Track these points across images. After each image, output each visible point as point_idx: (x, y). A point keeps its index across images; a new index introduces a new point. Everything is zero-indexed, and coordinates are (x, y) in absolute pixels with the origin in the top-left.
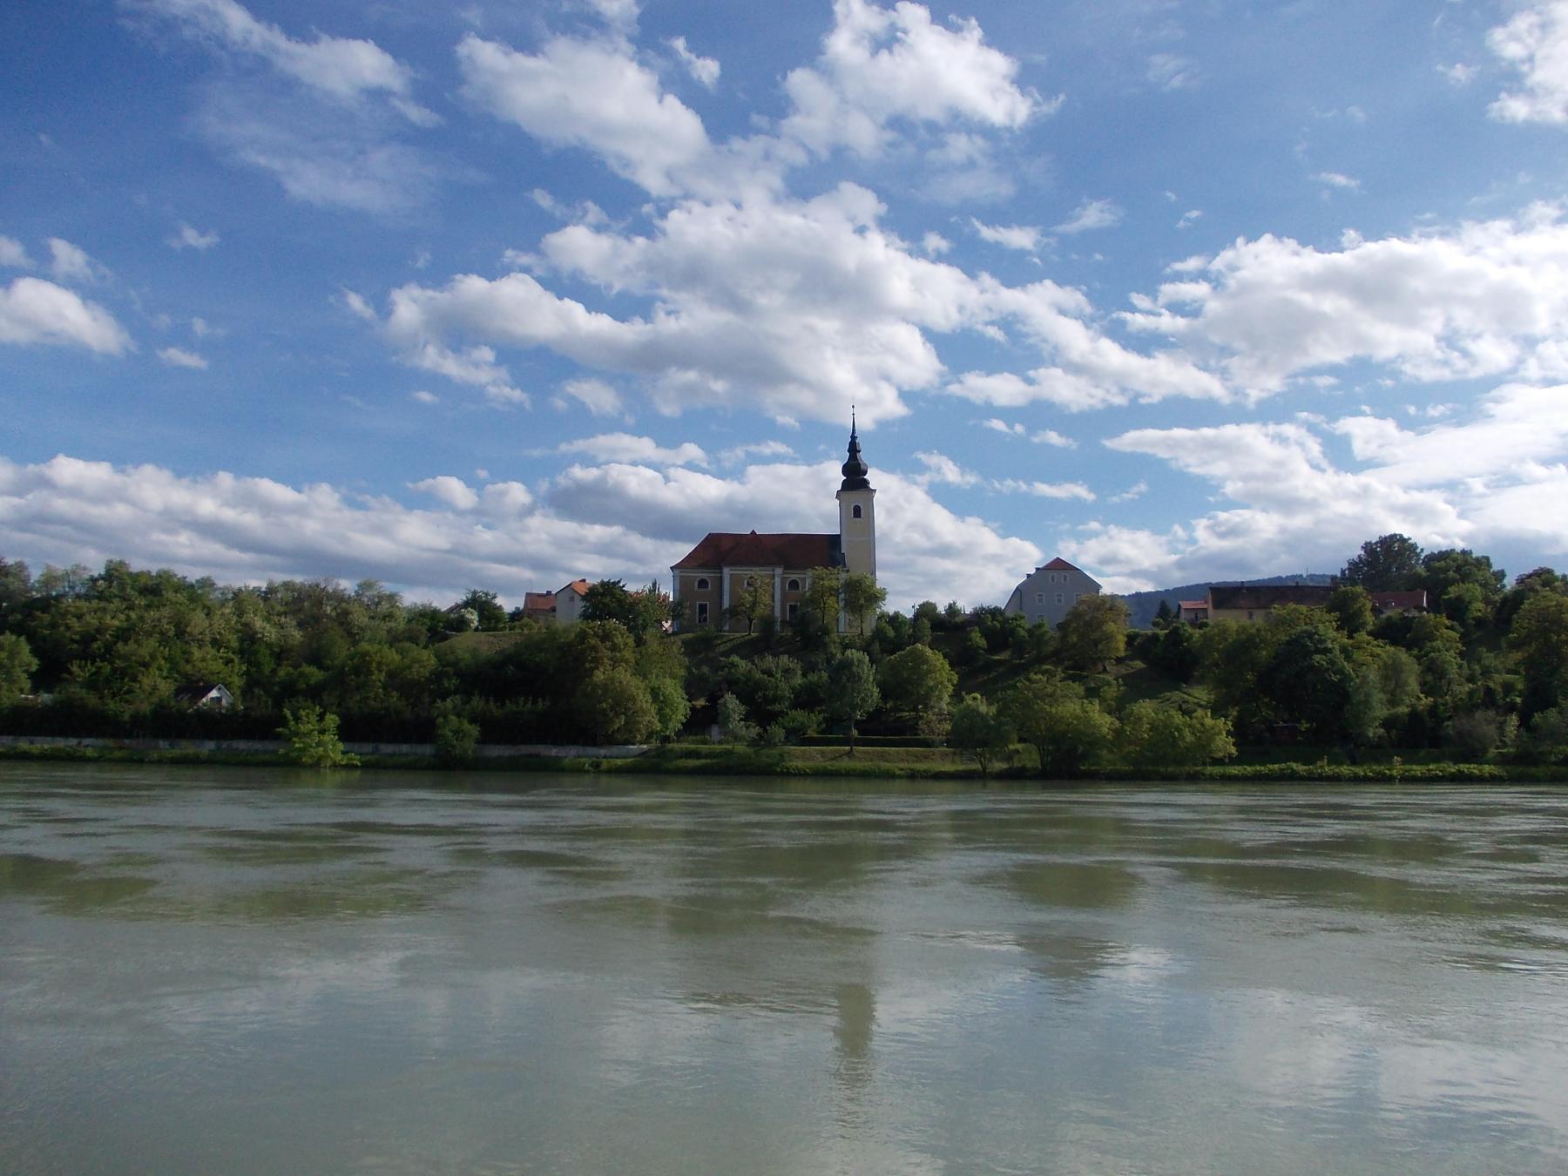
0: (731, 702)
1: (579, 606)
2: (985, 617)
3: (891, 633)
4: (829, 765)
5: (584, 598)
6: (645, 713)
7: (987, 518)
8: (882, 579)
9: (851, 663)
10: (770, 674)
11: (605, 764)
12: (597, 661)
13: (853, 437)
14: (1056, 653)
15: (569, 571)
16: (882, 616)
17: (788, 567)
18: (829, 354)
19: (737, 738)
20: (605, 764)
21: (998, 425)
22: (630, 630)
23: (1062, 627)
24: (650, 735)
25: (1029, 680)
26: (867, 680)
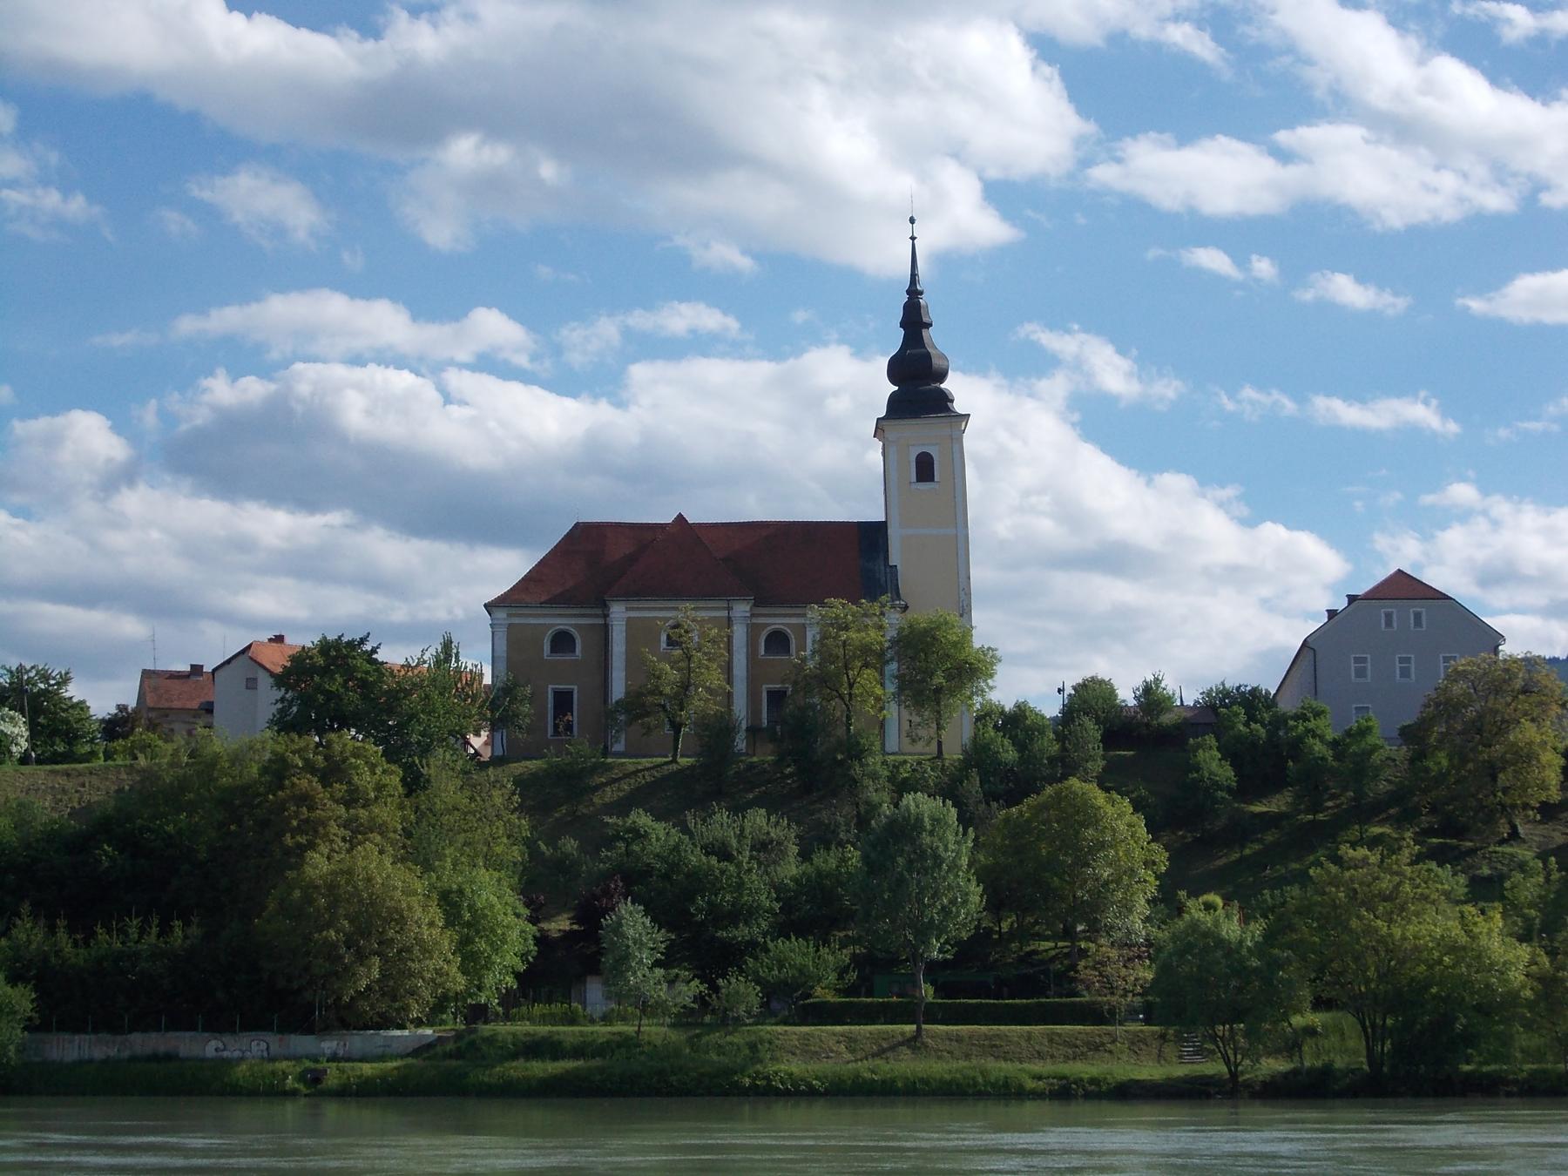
0: (633, 923)
1: (268, 699)
2: (1229, 710)
3: (1009, 754)
4: (865, 1069)
5: (281, 680)
6: (427, 951)
7: (1207, 475)
8: (987, 627)
9: (918, 823)
10: (724, 854)
11: (333, 1077)
12: (314, 829)
13: (914, 292)
14: (1398, 796)
15: (227, 618)
16: (986, 715)
17: (763, 599)
18: (818, 97)
19: (647, 1008)
20: (333, 1077)
21: (1213, 260)
22: (391, 755)
23: (1408, 734)
24: (440, 1006)
25: (1337, 860)
26: (954, 867)
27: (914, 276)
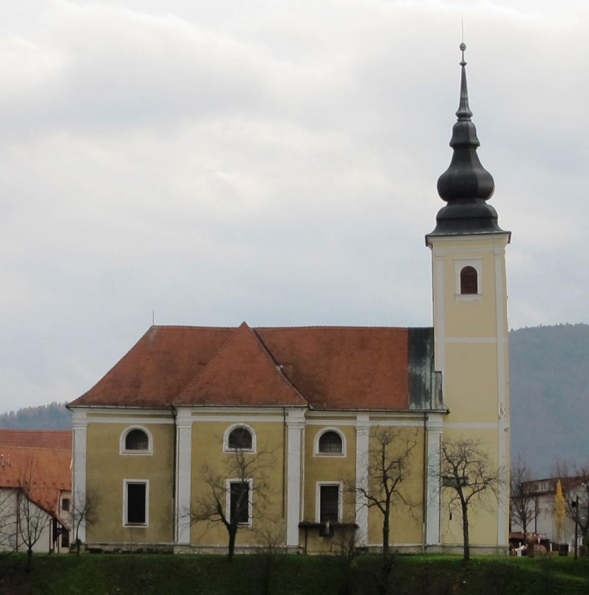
27: (464, 102)
